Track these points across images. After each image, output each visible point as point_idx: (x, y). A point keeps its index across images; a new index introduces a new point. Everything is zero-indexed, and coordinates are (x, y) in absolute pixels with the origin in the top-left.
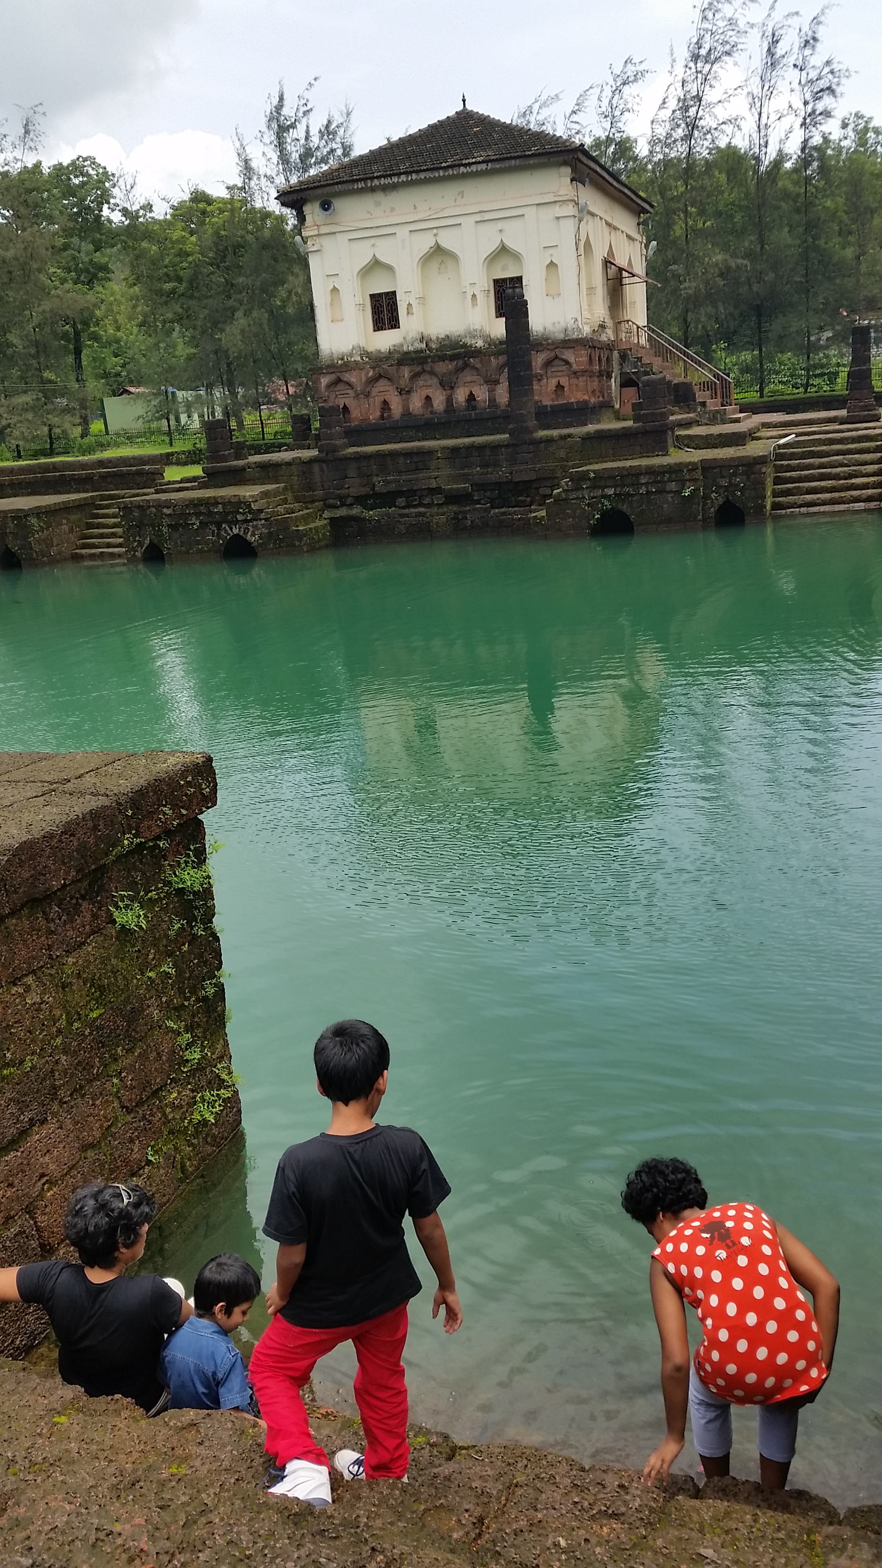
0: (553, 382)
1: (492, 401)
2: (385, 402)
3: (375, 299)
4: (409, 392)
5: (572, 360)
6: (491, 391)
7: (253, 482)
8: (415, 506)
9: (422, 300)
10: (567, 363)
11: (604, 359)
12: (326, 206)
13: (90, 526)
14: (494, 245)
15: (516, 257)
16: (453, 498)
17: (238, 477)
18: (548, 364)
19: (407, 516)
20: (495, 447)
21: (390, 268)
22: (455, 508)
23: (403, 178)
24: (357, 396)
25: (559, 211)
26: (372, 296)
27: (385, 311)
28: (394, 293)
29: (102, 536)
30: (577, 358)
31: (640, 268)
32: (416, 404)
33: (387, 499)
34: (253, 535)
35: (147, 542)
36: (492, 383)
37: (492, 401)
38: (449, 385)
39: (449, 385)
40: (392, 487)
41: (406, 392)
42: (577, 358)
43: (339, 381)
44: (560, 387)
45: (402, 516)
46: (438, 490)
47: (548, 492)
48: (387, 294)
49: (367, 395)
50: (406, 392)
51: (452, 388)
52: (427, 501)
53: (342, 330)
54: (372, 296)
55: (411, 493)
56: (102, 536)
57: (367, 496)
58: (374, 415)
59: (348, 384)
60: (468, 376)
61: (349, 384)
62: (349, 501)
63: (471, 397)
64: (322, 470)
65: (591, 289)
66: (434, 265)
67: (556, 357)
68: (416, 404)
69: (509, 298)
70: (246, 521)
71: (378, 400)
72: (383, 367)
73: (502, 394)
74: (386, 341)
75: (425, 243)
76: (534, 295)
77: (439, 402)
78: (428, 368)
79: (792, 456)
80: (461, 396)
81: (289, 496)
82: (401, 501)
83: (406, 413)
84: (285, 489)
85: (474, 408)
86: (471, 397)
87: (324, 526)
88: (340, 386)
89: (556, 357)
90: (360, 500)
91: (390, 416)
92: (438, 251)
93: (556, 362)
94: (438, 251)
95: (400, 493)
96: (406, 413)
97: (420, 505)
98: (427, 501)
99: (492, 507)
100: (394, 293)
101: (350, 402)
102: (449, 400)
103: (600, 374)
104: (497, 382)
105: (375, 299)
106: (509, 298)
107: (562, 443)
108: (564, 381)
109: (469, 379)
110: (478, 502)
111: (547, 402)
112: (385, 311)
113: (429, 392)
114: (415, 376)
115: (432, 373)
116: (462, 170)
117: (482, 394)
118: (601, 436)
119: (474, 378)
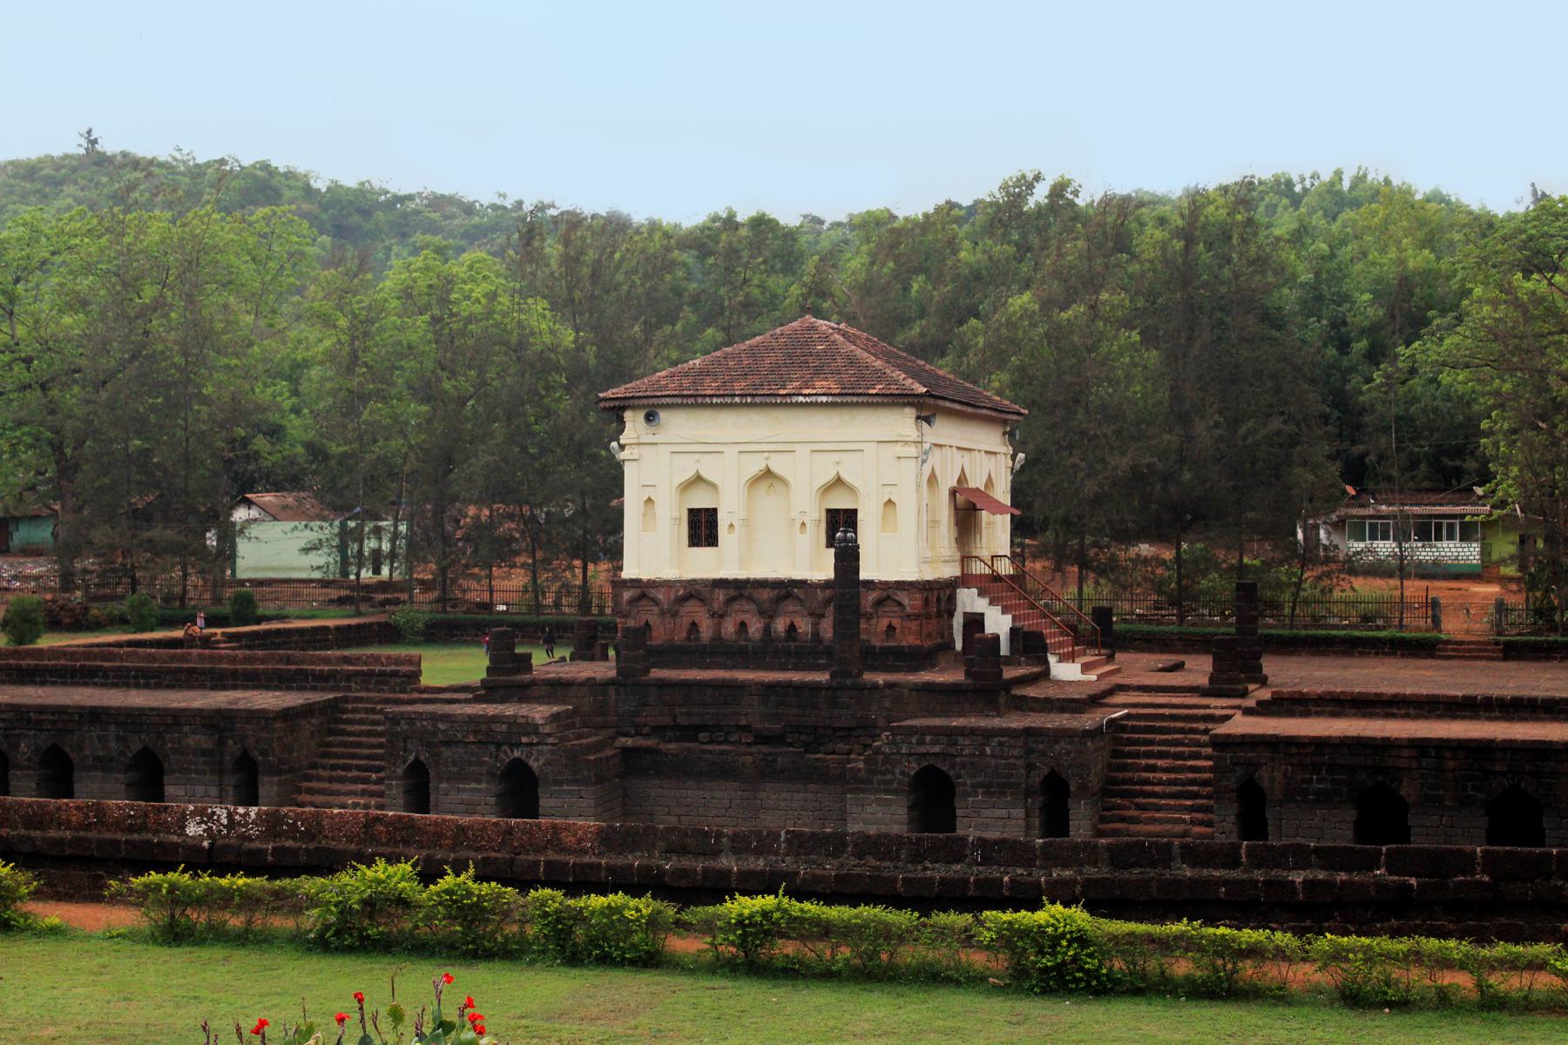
0: (885, 622)
1: (816, 634)
2: (694, 624)
3: (693, 513)
4: (722, 616)
5: (906, 601)
6: (815, 625)
7: (539, 700)
8: (720, 743)
9: (746, 522)
10: (900, 604)
11: (944, 598)
12: (650, 418)
13: (332, 732)
14: (829, 476)
15: (852, 490)
16: (762, 739)
17: (524, 692)
18: (879, 603)
19: (710, 752)
20: (815, 688)
21: (713, 486)
22: (765, 749)
23: (737, 400)
24: (663, 613)
25: (899, 450)
26: (691, 511)
27: (703, 528)
28: (715, 510)
29: (345, 744)
30: (909, 601)
31: (1002, 494)
32: (729, 628)
33: (689, 732)
34: (537, 760)
35: (412, 758)
36: (817, 616)
37: (816, 634)
38: (768, 614)
39: (768, 614)
40: (696, 720)
41: (719, 616)
42: (909, 601)
43: (643, 596)
44: (891, 628)
45: (704, 752)
46: (746, 728)
47: (869, 741)
48: (707, 510)
49: (675, 615)
50: (719, 616)
51: (771, 617)
52: (734, 738)
53: (652, 551)
54: (691, 511)
55: (719, 728)
56: (345, 744)
57: (664, 728)
58: (680, 636)
59: (653, 600)
60: (790, 606)
61: (656, 602)
62: (646, 730)
63: (792, 628)
64: (618, 694)
65: (934, 523)
66: (763, 487)
67: (889, 597)
68: (729, 628)
69: (841, 524)
70: (530, 745)
71: (686, 621)
72: (694, 591)
73: (827, 629)
74: (704, 565)
75: (755, 466)
76: (868, 537)
77: (755, 628)
78: (746, 593)
79: (1135, 729)
80: (780, 625)
81: (578, 720)
82: (703, 736)
83: (717, 637)
84: (575, 711)
85: (794, 639)
86: (792, 628)
87: (614, 756)
88: (644, 602)
89: (889, 597)
90: (658, 730)
91: (697, 639)
92: (768, 474)
93: (889, 602)
94: (768, 474)
95: (704, 728)
96: (717, 637)
97: (726, 741)
98: (734, 738)
99: (806, 752)
100: (715, 510)
101: (653, 619)
102: (767, 629)
103: (939, 615)
104: (822, 616)
105: (693, 513)
106: (841, 524)
107: (887, 692)
108: (896, 622)
109: (791, 608)
110: (791, 744)
111: (876, 642)
112: (703, 528)
113: (745, 617)
114: (730, 601)
115: (751, 599)
116: (801, 399)
117: (804, 626)
118: (930, 688)
119: (798, 608)
